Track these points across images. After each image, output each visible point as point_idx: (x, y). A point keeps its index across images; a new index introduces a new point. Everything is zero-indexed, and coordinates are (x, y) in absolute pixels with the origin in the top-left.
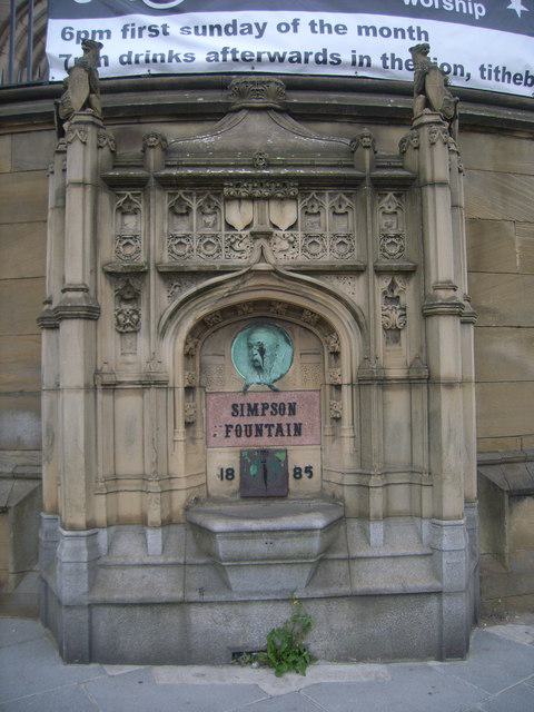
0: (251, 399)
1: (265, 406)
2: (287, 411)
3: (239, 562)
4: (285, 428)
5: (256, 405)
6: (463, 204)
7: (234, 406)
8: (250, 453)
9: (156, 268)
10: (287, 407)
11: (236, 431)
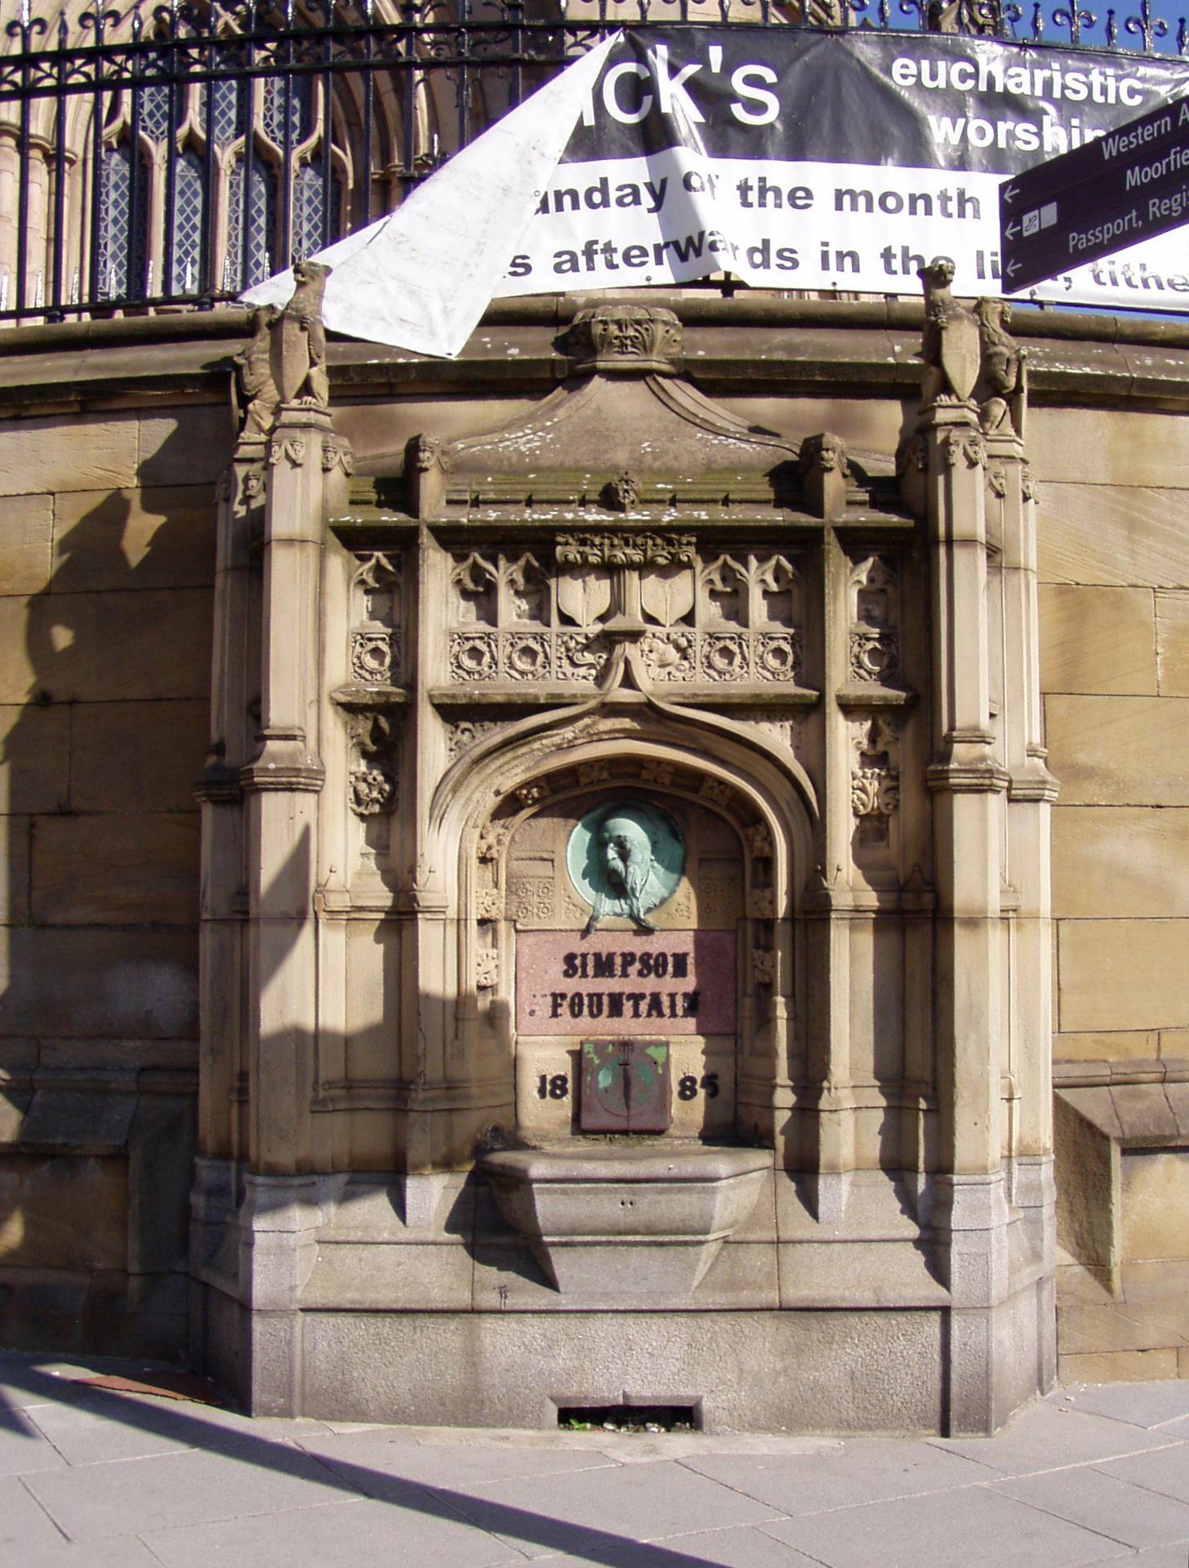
1: (628, 959)
2: (670, 969)
3: (579, 1237)
4: (665, 1001)
5: (611, 956)
6: (1033, 563)
7: (570, 958)
8: (600, 1047)
9: (431, 697)
10: (670, 960)
11: (572, 1006)
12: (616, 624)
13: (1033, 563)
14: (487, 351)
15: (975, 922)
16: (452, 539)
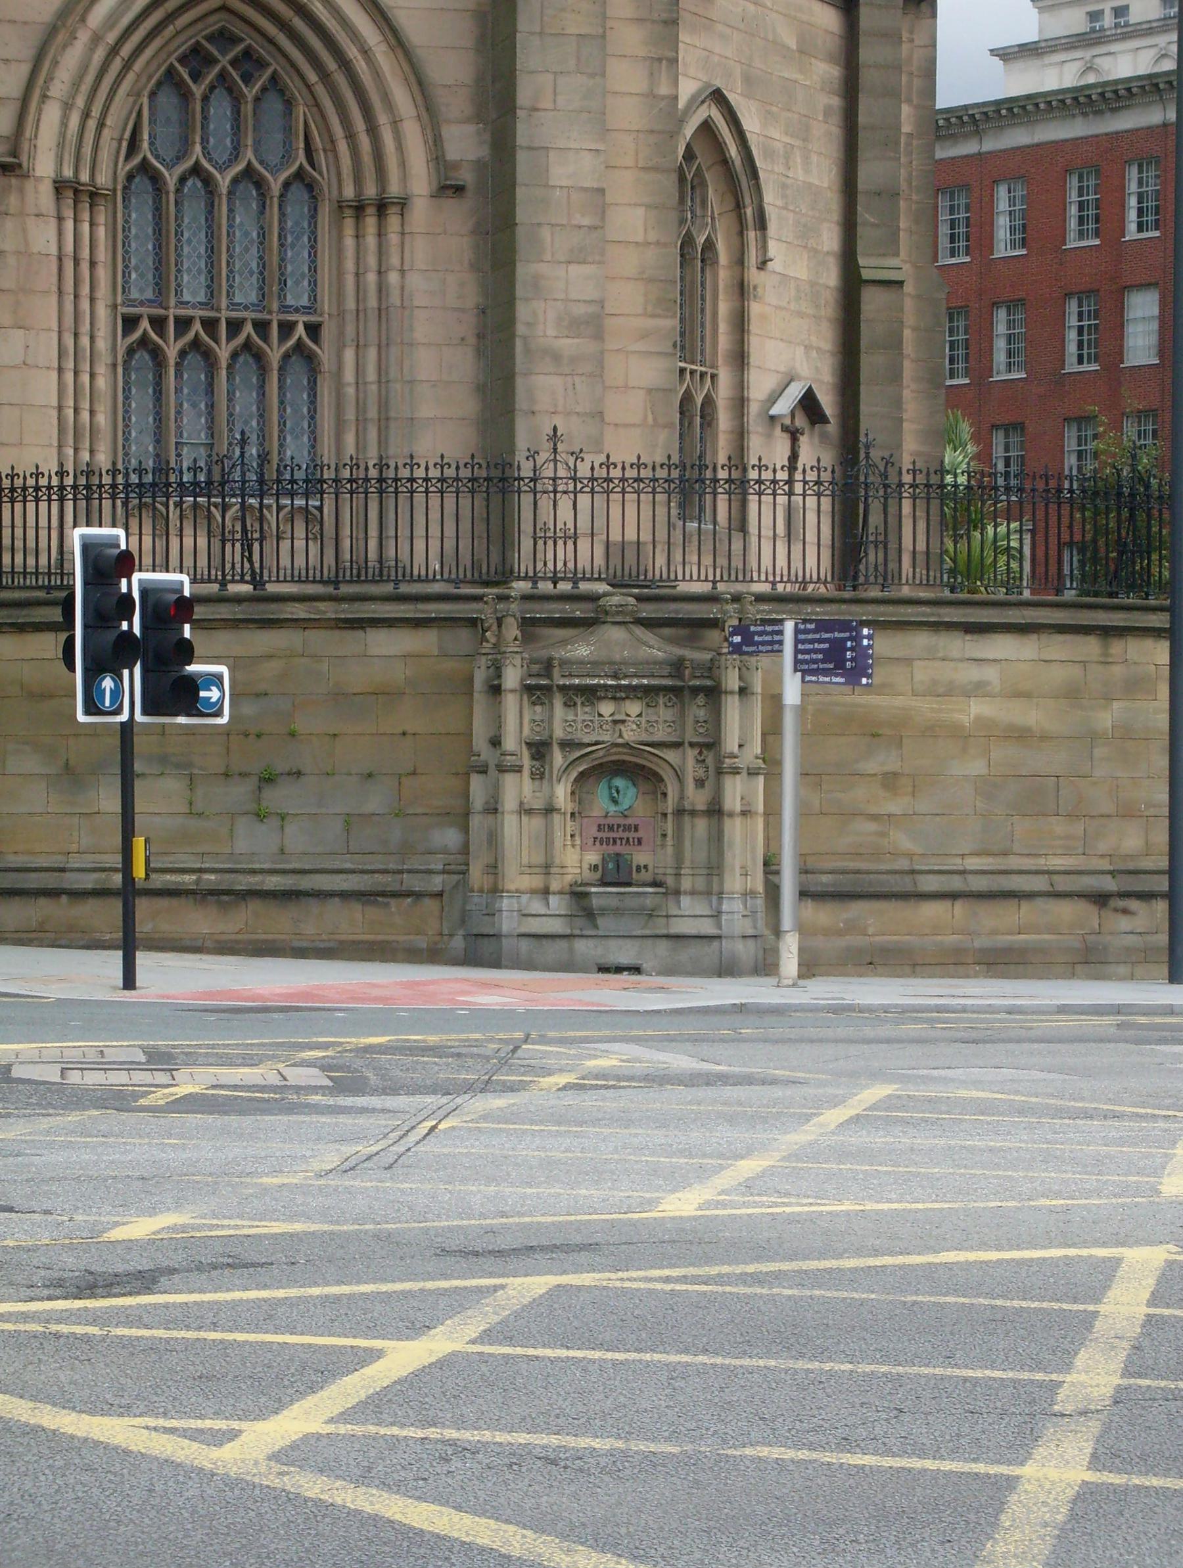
0: (610, 821)
1: (619, 826)
7: (599, 826)
8: (609, 855)
12: (617, 717)
13: (759, 690)
14: (567, 613)
15: (731, 815)
16: (563, 689)
